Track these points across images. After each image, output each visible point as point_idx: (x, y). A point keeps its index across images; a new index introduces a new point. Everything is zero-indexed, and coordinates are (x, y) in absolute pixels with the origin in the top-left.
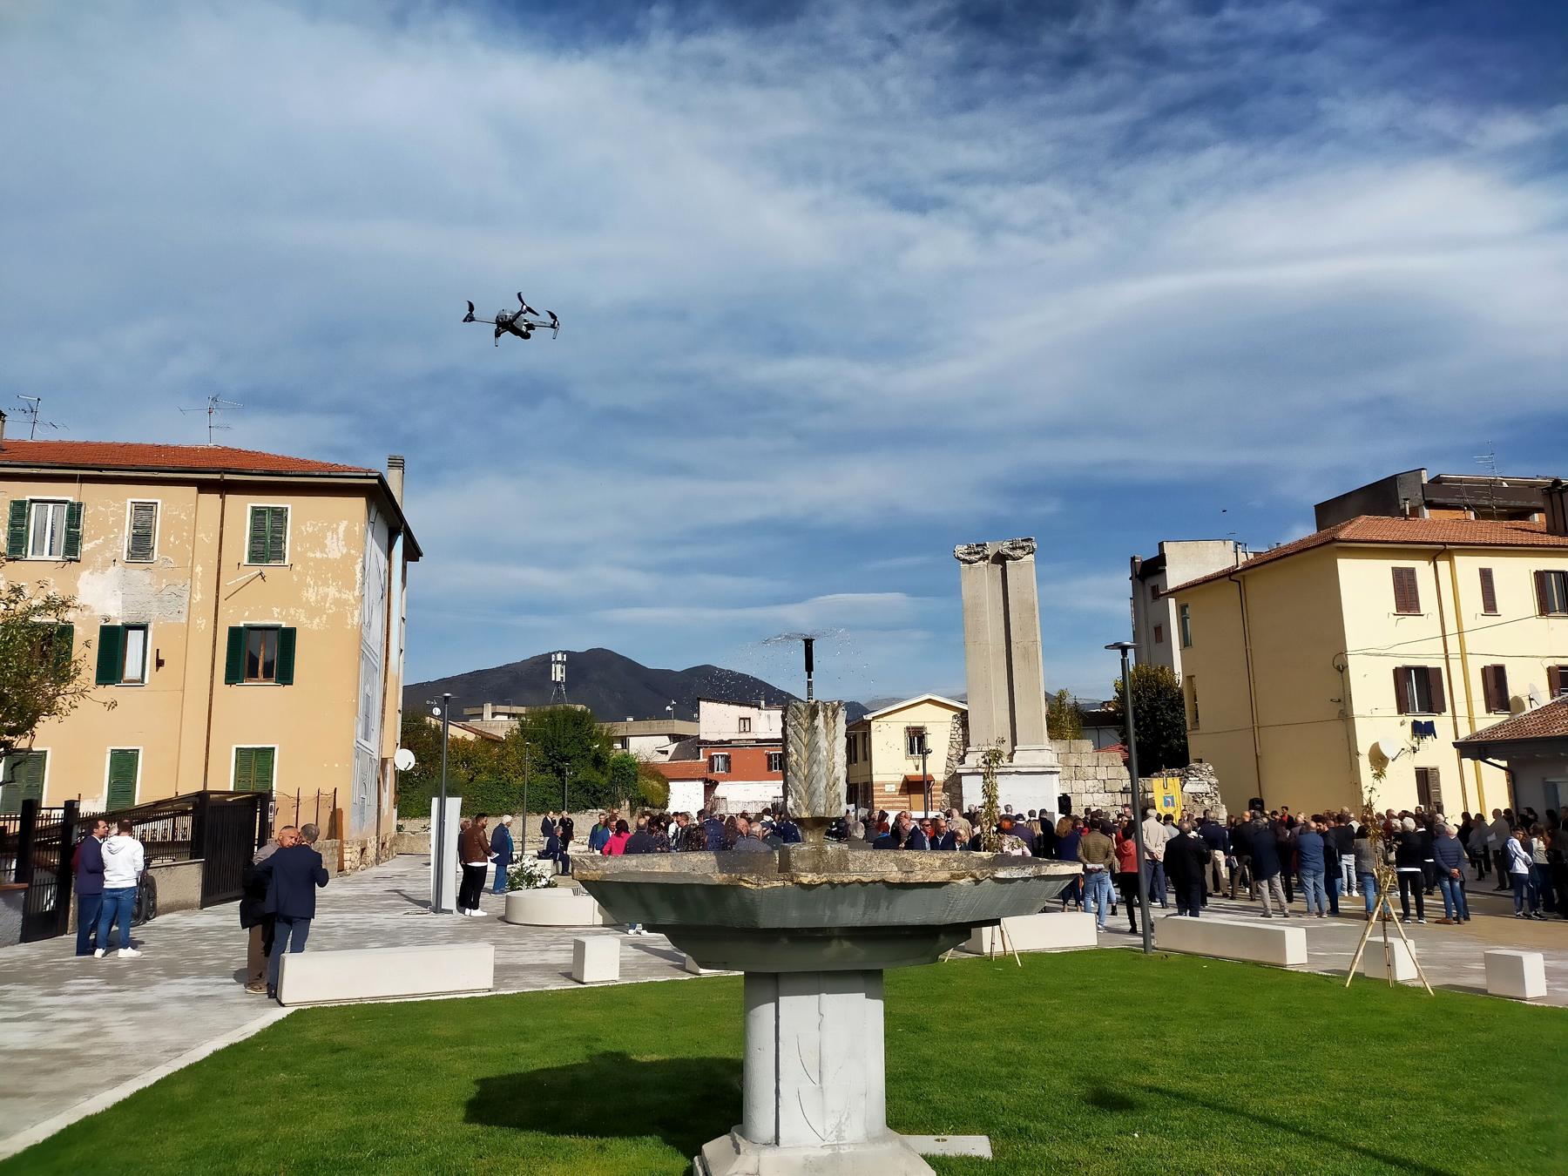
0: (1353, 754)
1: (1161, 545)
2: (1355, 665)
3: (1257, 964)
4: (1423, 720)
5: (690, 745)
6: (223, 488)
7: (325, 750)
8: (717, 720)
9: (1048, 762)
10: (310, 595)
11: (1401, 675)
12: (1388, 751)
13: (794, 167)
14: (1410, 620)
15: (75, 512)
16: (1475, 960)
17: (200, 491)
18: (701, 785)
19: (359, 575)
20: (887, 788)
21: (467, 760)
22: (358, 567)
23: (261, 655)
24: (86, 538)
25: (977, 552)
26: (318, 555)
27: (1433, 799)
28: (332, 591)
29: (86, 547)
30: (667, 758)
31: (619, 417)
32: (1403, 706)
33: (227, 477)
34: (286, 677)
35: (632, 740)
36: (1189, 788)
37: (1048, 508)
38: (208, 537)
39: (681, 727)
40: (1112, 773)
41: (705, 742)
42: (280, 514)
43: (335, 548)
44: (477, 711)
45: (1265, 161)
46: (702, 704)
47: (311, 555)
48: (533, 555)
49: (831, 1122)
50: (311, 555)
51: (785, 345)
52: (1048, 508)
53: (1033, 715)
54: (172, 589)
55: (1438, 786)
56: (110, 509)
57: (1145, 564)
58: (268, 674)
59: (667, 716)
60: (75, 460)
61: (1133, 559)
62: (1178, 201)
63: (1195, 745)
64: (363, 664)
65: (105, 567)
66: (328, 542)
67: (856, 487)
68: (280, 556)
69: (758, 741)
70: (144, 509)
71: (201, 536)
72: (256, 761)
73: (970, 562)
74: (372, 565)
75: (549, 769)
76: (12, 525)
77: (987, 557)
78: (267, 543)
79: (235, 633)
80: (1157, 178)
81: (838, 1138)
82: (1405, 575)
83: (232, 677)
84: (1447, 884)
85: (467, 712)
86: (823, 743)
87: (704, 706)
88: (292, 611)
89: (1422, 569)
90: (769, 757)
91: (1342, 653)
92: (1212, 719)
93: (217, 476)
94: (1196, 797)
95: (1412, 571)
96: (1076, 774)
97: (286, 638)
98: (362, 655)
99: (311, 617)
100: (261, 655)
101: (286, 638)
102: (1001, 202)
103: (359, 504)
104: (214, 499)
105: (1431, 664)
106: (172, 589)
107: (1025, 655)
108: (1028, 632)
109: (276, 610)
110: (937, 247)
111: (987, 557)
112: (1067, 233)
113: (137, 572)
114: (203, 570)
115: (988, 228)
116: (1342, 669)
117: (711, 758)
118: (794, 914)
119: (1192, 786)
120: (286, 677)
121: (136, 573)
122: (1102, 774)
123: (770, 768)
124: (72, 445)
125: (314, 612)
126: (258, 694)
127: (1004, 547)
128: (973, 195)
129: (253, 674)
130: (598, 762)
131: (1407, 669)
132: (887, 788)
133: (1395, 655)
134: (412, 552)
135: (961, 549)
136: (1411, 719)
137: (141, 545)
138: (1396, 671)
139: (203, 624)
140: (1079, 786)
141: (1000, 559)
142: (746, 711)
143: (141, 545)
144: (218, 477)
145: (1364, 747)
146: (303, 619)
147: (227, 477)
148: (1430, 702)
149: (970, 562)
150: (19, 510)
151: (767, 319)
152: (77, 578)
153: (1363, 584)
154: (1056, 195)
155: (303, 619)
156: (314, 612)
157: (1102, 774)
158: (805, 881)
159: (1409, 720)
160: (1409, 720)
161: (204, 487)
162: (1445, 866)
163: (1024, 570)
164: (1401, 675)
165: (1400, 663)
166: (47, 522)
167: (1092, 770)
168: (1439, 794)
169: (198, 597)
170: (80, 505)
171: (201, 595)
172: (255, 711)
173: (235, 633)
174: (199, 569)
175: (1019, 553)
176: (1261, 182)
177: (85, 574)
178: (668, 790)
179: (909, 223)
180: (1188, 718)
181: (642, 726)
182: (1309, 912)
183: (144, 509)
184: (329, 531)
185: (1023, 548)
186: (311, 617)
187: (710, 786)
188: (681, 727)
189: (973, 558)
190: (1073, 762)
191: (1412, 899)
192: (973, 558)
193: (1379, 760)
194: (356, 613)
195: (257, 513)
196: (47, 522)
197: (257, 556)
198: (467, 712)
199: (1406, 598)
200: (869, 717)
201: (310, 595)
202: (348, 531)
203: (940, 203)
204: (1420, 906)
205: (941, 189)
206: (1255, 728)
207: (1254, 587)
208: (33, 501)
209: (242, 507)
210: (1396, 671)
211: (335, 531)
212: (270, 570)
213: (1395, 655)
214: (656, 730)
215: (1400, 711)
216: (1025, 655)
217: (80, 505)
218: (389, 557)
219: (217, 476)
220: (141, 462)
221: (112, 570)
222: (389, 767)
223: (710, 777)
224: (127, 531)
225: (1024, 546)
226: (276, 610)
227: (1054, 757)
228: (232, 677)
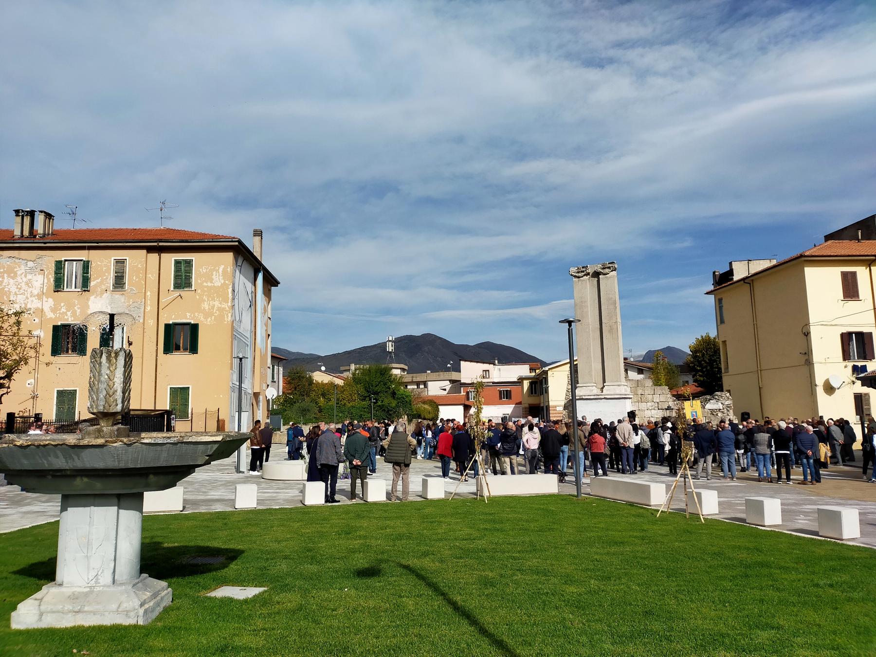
0: (812, 385)
1: (731, 264)
2: (814, 332)
3: (632, 504)
4: (860, 364)
5: (457, 384)
6: (160, 250)
7: (217, 390)
8: (470, 371)
9: (623, 392)
10: (206, 306)
11: (846, 338)
12: (835, 384)
13: (523, 46)
14: (852, 304)
15: (86, 266)
16: (741, 504)
17: (148, 252)
18: (461, 408)
19: (230, 295)
20: (558, 409)
21: (323, 395)
22: (230, 290)
23: (181, 338)
24: (92, 279)
25: (583, 271)
26: (209, 284)
27: (865, 412)
28: (217, 303)
29: (92, 284)
30: (445, 393)
31: (430, 201)
32: (846, 356)
33: (161, 244)
34: (193, 348)
35: (430, 383)
36: (709, 406)
37: (688, 243)
38: (152, 277)
39: (454, 376)
40: (663, 398)
41: (465, 384)
42: (189, 263)
43: (218, 280)
44: (347, 368)
45: (818, 18)
46: (462, 363)
47: (205, 284)
48: (386, 282)
49: (93, 574)
50: (205, 284)
51: (522, 156)
52: (688, 243)
53: (615, 365)
54: (136, 304)
55: (869, 404)
56: (103, 263)
57: (722, 275)
58: (185, 349)
59: (448, 370)
60: (86, 238)
61: (714, 273)
62: (763, 49)
63: (726, 381)
64: (235, 342)
65: (102, 294)
66: (214, 277)
67: (569, 237)
68: (189, 285)
69: (493, 383)
70: (120, 262)
71: (149, 276)
72: (180, 395)
73: (579, 277)
74: (240, 288)
75: (367, 399)
76: (56, 273)
77: (588, 274)
78: (183, 280)
79: (168, 327)
80: (750, 36)
81: (96, 582)
82: (849, 277)
83: (168, 350)
84: (805, 461)
85: (342, 368)
86: (105, 371)
87: (464, 364)
88: (196, 314)
89: (862, 272)
90: (500, 392)
91: (807, 324)
92: (736, 365)
93: (155, 244)
94: (713, 412)
95: (854, 274)
96: (642, 399)
97: (194, 329)
98: (233, 337)
99: (206, 318)
100: (181, 338)
101: (194, 329)
102: (650, 58)
103: (229, 256)
104: (154, 257)
105: (865, 330)
106: (136, 304)
107: (611, 330)
108: (615, 318)
109: (188, 314)
110: (611, 88)
111: (588, 274)
112: (692, 74)
113: (117, 296)
114: (151, 294)
115: (642, 75)
116: (807, 334)
117: (468, 393)
118: (25, 462)
119: (711, 405)
120: (194, 349)
121: (117, 296)
122: (657, 398)
123: (501, 398)
124: (107, 230)
125: (207, 315)
126: (180, 359)
127: (598, 268)
128: (632, 55)
129: (178, 348)
130: (394, 394)
131: (850, 334)
132: (558, 409)
133: (842, 325)
134: (271, 281)
135: (573, 270)
136: (852, 364)
137: (119, 282)
138: (842, 335)
139: (152, 322)
140: (643, 406)
141: (596, 275)
142: (486, 366)
143: (119, 282)
144: (157, 244)
145: (820, 381)
146: (202, 319)
147: (161, 244)
148: (864, 352)
149: (579, 277)
150: (59, 265)
151: (512, 141)
152: (88, 299)
153: (821, 283)
154: (684, 51)
155: (202, 319)
156: (207, 315)
157: (657, 398)
158: (18, 444)
159: (850, 364)
160: (850, 364)
161: (150, 250)
162: (803, 449)
163: (611, 282)
164: (846, 338)
165: (845, 330)
166: (73, 271)
167: (650, 397)
168: (869, 409)
169: (148, 308)
170: (88, 262)
171: (151, 308)
172: (179, 368)
173: (168, 327)
174: (148, 293)
175: (607, 270)
176: (818, 32)
177: (92, 298)
178: (438, 411)
179: (593, 75)
180: (723, 366)
181: (435, 375)
182: (724, 477)
183: (120, 262)
184: (214, 270)
185: (609, 268)
186: (206, 318)
187: (467, 408)
188: (454, 376)
189: (580, 275)
190: (640, 392)
191: (783, 471)
192: (580, 275)
193: (830, 389)
194: (230, 315)
195: (177, 263)
196: (73, 271)
197: (177, 286)
198: (342, 368)
199: (850, 289)
200: (547, 368)
201: (206, 306)
202: (224, 271)
203: (611, 61)
204: (788, 475)
205: (612, 53)
206: (759, 371)
207: (758, 286)
208: (66, 260)
209: (170, 260)
210: (842, 335)
211: (217, 271)
212: (185, 293)
213: (842, 325)
214: (442, 377)
215: (844, 359)
216: (611, 330)
217: (88, 262)
218: (255, 285)
219: (155, 244)
220: (129, 237)
221: (105, 295)
222: (261, 398)
223: (467, 403)
224: (112, 275)
225: (610, 266)
226: (188, 314)
227: (629, 390)
228: (168, 350)
